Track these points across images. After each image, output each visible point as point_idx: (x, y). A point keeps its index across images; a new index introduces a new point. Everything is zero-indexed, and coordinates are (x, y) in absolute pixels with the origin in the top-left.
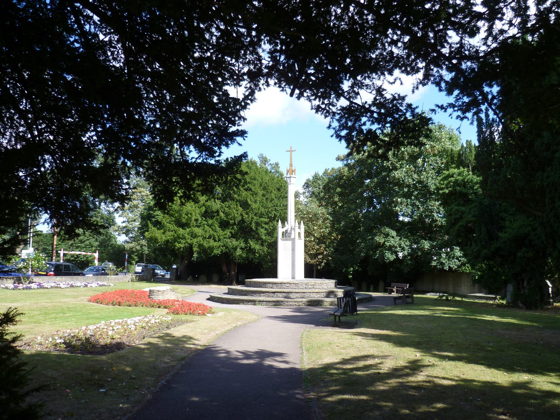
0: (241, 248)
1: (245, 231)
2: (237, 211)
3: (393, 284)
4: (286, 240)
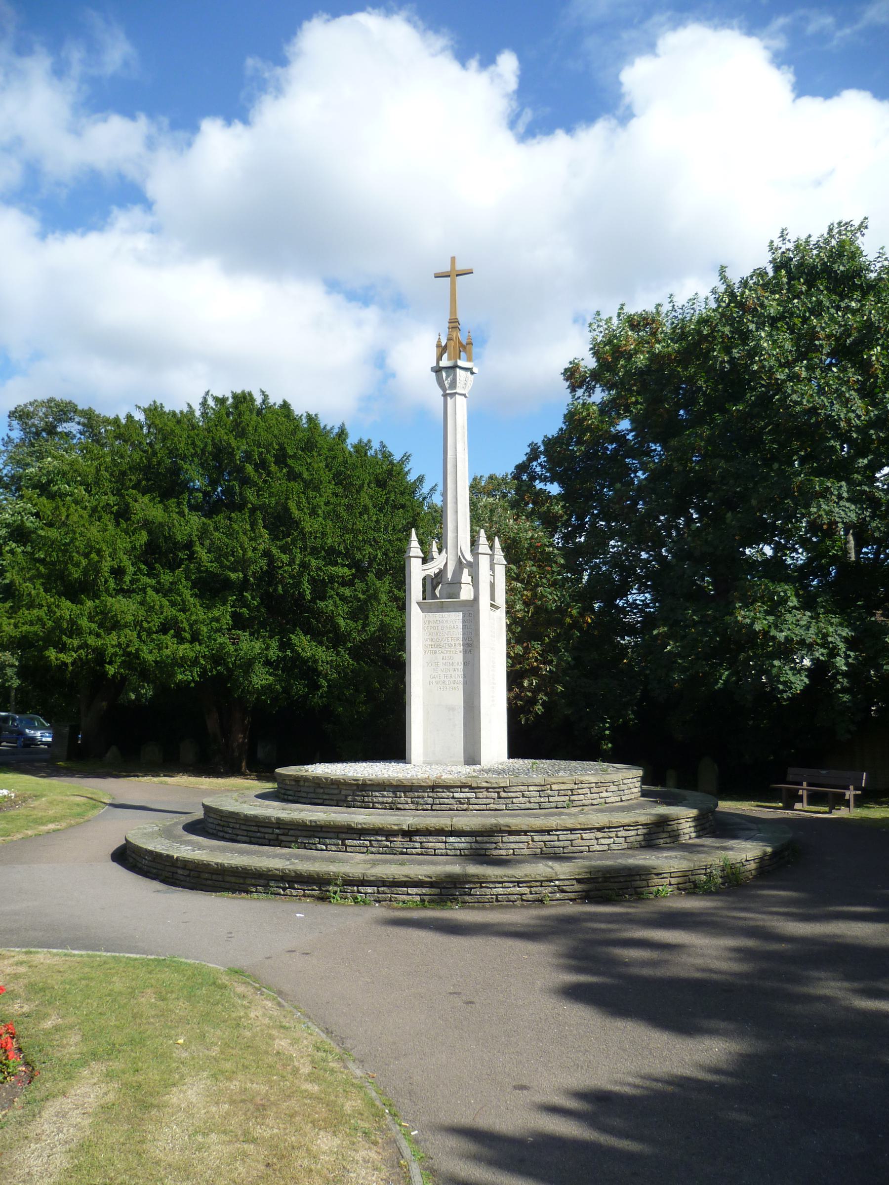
1: (280, 608)
4: (442, 608)
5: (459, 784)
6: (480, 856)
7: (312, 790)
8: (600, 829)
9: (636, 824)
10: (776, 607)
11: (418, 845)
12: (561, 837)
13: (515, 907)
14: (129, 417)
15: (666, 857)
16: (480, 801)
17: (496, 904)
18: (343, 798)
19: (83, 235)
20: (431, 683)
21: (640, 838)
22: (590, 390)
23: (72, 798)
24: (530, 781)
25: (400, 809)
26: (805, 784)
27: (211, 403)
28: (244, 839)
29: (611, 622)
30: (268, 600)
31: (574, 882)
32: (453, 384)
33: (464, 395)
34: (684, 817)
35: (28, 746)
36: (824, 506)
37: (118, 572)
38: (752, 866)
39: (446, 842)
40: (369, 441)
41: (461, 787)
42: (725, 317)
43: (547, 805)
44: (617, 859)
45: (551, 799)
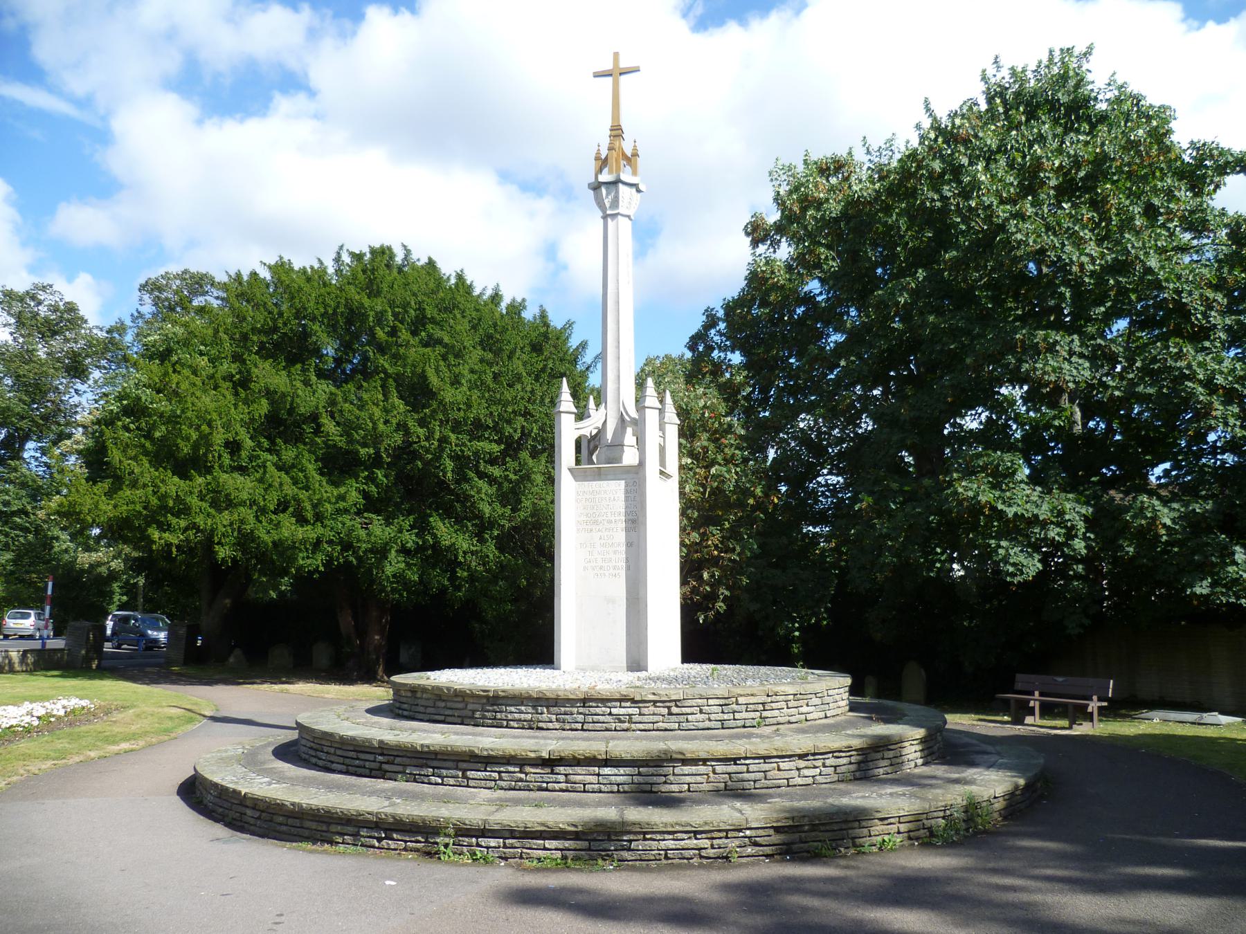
0: (404, 551)
1: (415, 487)
2: (386, 411)
3: (1021, 680)
4: (599, 475)
5: (618, 696)
6: (647, 795)
7: (430, 703)
8: (802, 757)
9: (849, 749)
10: (1001, 478)
11: (562, 778)
12: (752, 768)
13: (691, 867)
14: (254, 274)
15: (891, 794)
16: (645, 719)
17: (664, 862)
18: (470, 714)
19: (242, 121)
20: (585, 568)
21: (853, 767)
22: (775, 244)
23: (166, 710)
24: (710, 693)
25: (542, 729)
26: (1037, 693)
27: (346, 259)
28: (340, 767)
29: (801, 507)
30: (403, 479)
31: (771, 832)
32: (615, 203)
33: (629, 217)
34: (910, 737)
35: (150, 649)
36: (1051, 362)
37: (233, 447)
38: (999, 805)
39: (598, 775)
40: (524, 300)
41: (620, 700)
42: (934, 152)
43: (732, 723)
44: (827, 797)
45: (737, 716)
